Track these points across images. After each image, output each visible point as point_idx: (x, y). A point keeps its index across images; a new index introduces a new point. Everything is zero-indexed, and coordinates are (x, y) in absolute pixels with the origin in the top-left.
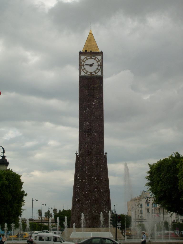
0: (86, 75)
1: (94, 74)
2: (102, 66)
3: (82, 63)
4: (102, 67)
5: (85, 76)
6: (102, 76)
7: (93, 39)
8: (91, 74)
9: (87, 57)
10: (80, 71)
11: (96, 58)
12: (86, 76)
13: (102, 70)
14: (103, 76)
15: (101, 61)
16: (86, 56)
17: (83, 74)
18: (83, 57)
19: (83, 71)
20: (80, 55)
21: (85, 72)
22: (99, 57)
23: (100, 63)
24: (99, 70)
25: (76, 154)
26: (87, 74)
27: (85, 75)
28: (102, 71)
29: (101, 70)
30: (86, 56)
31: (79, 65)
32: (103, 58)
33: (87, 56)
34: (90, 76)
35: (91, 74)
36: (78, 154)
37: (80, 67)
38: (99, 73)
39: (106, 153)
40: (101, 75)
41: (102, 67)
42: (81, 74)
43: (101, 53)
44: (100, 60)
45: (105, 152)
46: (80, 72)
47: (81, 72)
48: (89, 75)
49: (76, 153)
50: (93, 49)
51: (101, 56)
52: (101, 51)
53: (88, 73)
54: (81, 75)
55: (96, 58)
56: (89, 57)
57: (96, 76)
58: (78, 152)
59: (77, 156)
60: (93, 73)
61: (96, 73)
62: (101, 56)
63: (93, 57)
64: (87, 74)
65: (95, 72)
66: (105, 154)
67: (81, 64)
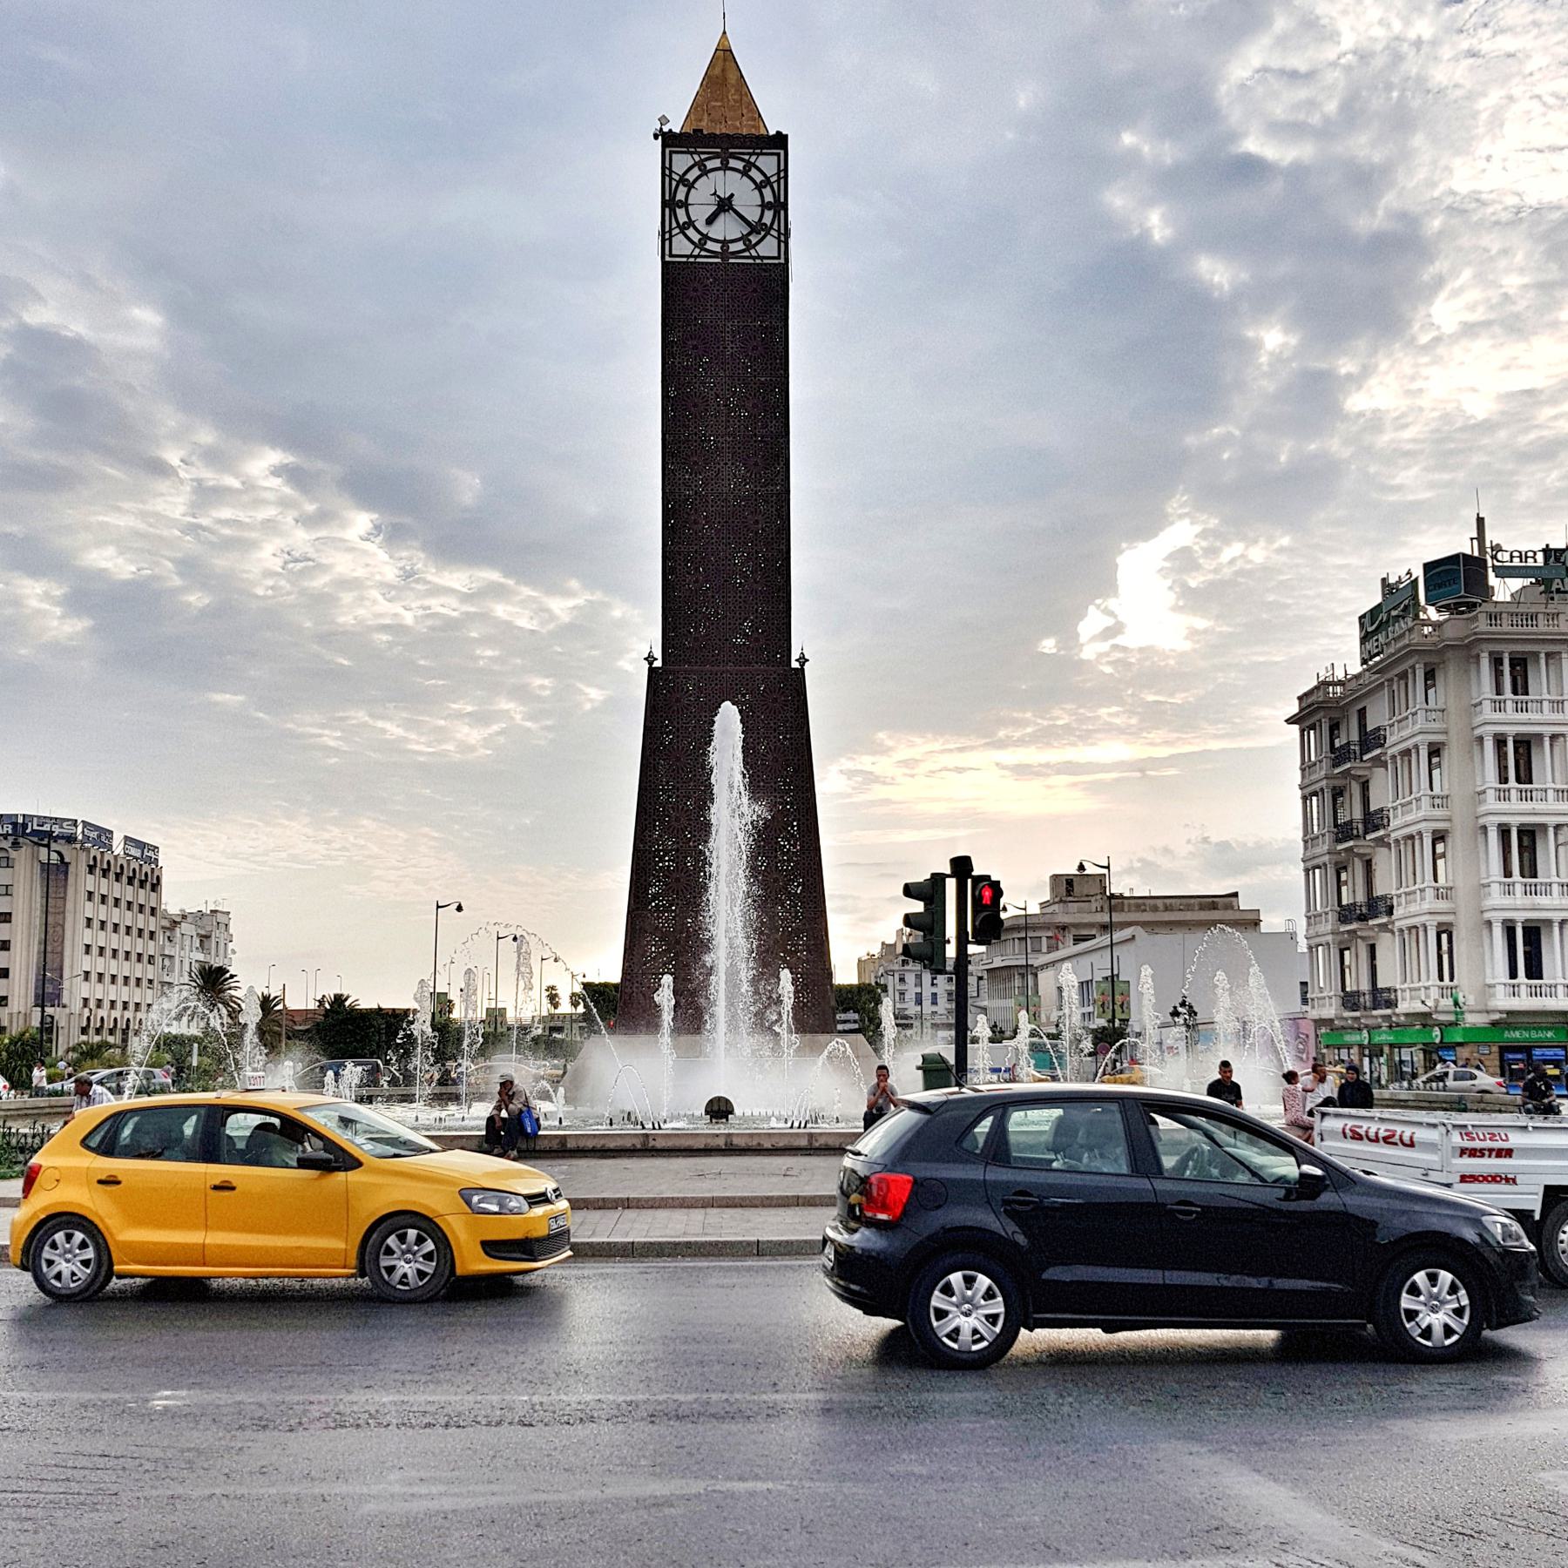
0: (699, 256)
1: (743, 251)
2: (670, 204)
4: (782, 212)
5: (692, 260)
6: (782, 261)
7: (732, 78)
8: (725, 254)
9: (707, 159)
10: (670, 232)
11: (750, 165)
12: (699, 260)
13: (667, 179)
14: (787, 259)
15: (671, 229)
16: (699, 154)
17: (682, 246)
18: (681, 162)
19: (681, 236)
20: (667, 150)
22: (768, 164)
24: (682, 180)
25: (651, 663)
26: (743, 160)
27: (758, 154)
30: (753, 253)
31: (664, 204)
34: (719, 260)
35: (725, 254)
36: (658, 664)
38: (768, 248)
39: (803, 660)
40: (778, 257)
41: (782, 212)
42: (674, 252)
43: (780, 141)
44: (775, 178)
45: (795, 655)
47: (671, 236)
48: (714, 254)
49: (650, 659)
51: (671, 255)
52: (779, 133)
53: (740, 165)
54: (671, 255)
55: (750, 165)
56: (716, 163)
57: (751, 261)
58: (658, 653)
59: (652, 671)
60: (733, 247)
61: (700, 165)
62: (778, 155)
63: (733, 163)
65: (705, 172)
66: (795, 665)
67: (776, 215)
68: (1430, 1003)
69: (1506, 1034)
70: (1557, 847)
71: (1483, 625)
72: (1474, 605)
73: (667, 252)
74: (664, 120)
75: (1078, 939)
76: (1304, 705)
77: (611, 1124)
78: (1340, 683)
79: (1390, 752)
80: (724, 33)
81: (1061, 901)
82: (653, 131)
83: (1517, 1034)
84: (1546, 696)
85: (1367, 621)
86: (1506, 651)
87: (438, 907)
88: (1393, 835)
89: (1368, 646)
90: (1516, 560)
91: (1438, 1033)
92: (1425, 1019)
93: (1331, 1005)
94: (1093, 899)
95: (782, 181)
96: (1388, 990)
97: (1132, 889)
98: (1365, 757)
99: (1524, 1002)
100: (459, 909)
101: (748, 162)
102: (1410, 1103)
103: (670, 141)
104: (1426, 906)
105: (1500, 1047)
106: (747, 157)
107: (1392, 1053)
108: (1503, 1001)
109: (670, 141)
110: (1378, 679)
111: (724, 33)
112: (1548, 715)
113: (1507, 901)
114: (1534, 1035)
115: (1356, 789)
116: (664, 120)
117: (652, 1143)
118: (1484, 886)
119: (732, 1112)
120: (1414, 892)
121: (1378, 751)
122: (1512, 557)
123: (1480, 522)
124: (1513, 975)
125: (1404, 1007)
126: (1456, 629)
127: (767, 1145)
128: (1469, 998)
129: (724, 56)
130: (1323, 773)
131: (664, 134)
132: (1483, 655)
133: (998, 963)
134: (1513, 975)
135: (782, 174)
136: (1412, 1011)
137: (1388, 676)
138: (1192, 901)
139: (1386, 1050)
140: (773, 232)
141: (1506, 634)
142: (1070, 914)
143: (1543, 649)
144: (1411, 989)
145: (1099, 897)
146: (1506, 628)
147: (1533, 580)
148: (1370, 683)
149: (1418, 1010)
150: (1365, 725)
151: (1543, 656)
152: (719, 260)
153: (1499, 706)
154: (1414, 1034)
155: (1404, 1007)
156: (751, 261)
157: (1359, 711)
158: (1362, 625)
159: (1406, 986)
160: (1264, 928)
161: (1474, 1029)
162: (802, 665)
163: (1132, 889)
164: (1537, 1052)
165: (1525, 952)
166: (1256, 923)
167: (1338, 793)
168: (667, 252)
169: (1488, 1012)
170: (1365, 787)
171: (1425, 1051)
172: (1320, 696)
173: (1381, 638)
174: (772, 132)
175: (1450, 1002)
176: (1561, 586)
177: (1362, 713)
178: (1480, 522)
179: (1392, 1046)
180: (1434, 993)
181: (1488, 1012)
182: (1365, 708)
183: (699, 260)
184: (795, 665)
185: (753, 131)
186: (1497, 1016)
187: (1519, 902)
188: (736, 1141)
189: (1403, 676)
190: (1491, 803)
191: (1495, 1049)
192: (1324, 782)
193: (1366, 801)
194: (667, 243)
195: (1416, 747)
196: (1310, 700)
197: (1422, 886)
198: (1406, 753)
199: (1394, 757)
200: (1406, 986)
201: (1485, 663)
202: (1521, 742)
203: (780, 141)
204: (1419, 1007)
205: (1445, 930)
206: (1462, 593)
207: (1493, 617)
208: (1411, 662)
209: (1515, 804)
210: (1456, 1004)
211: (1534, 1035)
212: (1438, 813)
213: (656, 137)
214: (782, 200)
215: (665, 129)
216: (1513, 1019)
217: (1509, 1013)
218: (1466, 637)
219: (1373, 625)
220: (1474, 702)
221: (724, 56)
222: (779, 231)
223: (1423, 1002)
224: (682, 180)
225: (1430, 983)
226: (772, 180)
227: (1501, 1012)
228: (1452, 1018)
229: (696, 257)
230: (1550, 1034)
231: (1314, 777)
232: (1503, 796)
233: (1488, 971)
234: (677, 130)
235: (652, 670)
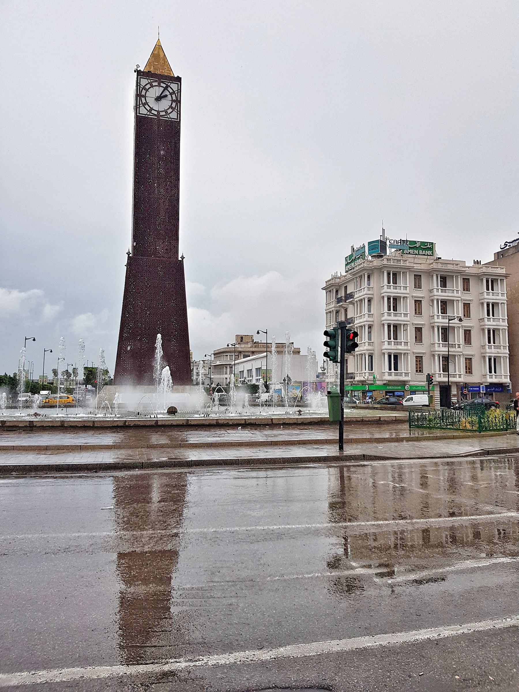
1: (152, 82)
2: (178, 102)
3: (176, 105)
4: (179, 104)
5: (147, 116)
6: (178, 120)
7: (162, 56)
8: (158, 115)
9: (152, 82)
10: (178, 92)
12: (149, 116)
13: (179, 110)
14: (180, 120)
17: (143, 111)
18: (144, 82)
19: (143, 107)
21: (148, 108)
22: (174, 87)
23: (141, 101)
24: (173, 109)
25: (129, 255)
26: (166, 84)
27: (171, 83)
28: (179, 113)
29: (177, 110)
30: (149, 81)
31: (180, 102)
32: (180, 90)
33: (152, 81)
35: (158, 115)
37: (179, 100)
38: (174, 115)
39: (183, 258)
41: (179, 104)
43: (179, 79)
45: (180, 256)
46: (179, 90)
47: (139, 107)
49: (128, 253)
50: (163, 71)
53: (153, 112)
55: (167, 86)
56: (156, 84)
57: (168, 119)
60: (161, 114)
62: (178, 84)
63: (156, 113)
64: (166, 84)
65: (152, 86)
66: (180, 259)
68: (366, 378)
69: (388, 387)
70: (403, 331)
71: (385, 262)
72: (382, 256)
73: (138, 112)
74: (138, 66)
75: (245, 356)
76: (328, 284)
77: (260, 413)
78: (339, 278)
79: (355, 300)
80: (159, 39)
81: (239, 344)
82: (134, 69)
83: (390, 388)
84: (402, 285)
85: (348, 259)
86: (439, 274)
87: (26, 339)
88: (355, 326)
89: (348, 266)
90: (395, 243)
91: (368, 387)
92: (363, 383)
93: (333, 378)
94: (249, 343)
95: (179, 93)
96: (352, 373)
97: (261, 341)
98: (347, 301)
99: (393, 378)
100: (34, 340)
101: (175, 108)
102: (378, 408)
103: (139, 73)
104: (365, 348)
105: (386, 391)
106: (167, 83)
107: (352, 393)
108: (387, 377)
109: (139, 73)
110: (352, 277)
111: (159, 39)
112: (402, 291)
113: (389, 347)
114: (396, 388)
115: (343, 311)
116: (138, 66)
117: (190, 423)
118: (383, 342)
119: (177, 412)
120: (362, 343)
121: (352, 299)
122: (394, 242)
123: (383, 230)
124: (390, 369)
125: (357, 379)
126: (377, 262)
127: (231, 423)
128: (378, 377)
129: (158, 48)
130: (333, 306)
131: (138, 71)
132: (385, 271)
133: (218, 363)
134: (390, 369)
135: (179, 91)
136: (360, 380)
137: (356, 276)
138: (280, 345)
139: (350, 392)
140: (175, 110)
141: (391, 265)
142: (240, 347)
143: (402, 271)
144: (360, 373)
145: (251, 343)
146: (392, 263)
147: (396, 249)
148: (349, 278)
149: (362, 380)
150: (346, 292)
151: (499, 280)
152: (156, 117)
153: (389, 287)
154: (360, 387)
155: (357, 379)
156: (168, 119)
157: (345, 287)
158: (346, 260)
159: (358, 372)
160: (301, 354)
161: (379, 386)
162: (183, 259)
163: (261, 341)
164: (396, 393)
165: (394, 363)
166: (299, 352)
167: (337, 312)
168: (138, 112)
169: (382, 381)
170: (346, 310)
171: (362, 392)
172: (333, 282)
173: (352, 264)
174: (176, 76)
175: (372, 377)
176: (425, 253)
177: (346, 288)
178: (383, 230)
179: (352, 391)
180: (367, 374)
181: (382, 381)
182: (347, 286)
183: (149, 116)
184: (180, 259)
185: (169, 74)
186: (385, 382)
187: (393, 347)
188: (220, 422)
189: (361, 277)
190: (386, 317)
191: (384, 392)
192: (334, 308)
193: (346, 315)
194: (179, 89)
195: (364, 299)
196: (330, 282)
197: (365, 342)
198: (361, 300)
199: (357, 301)
200: (358, 372)
201: (435, 277)
202: (394, 299)
203: (179, 79)
204: (362, 379)
205: (371, 356)
206: (379, 252)
207: (388, 260)
208: (364, 272)
209: (392, 317)
210: (374, 378)
211: (396, 388)
212: (370, 319)
213: (135, 71)
214: (179, 100)
215: (138, 69)
216: (389, 383)
217: (389, 381)
218: (381, 266)
219: (350, 260)
220: (381, 286)
221: (158, 48)
222: (177, 110)
223: (364, 377)
224: (173, 109)
225: (366, 371)
226: (176, 92)
227: (387, 381)
228: (372, 382)
229: (148, 115)
230: (400, 388)
231: (330, 307)
232: (389, 315)
233: (383, 368)
234: (142, 70)
235: (129, 257)
